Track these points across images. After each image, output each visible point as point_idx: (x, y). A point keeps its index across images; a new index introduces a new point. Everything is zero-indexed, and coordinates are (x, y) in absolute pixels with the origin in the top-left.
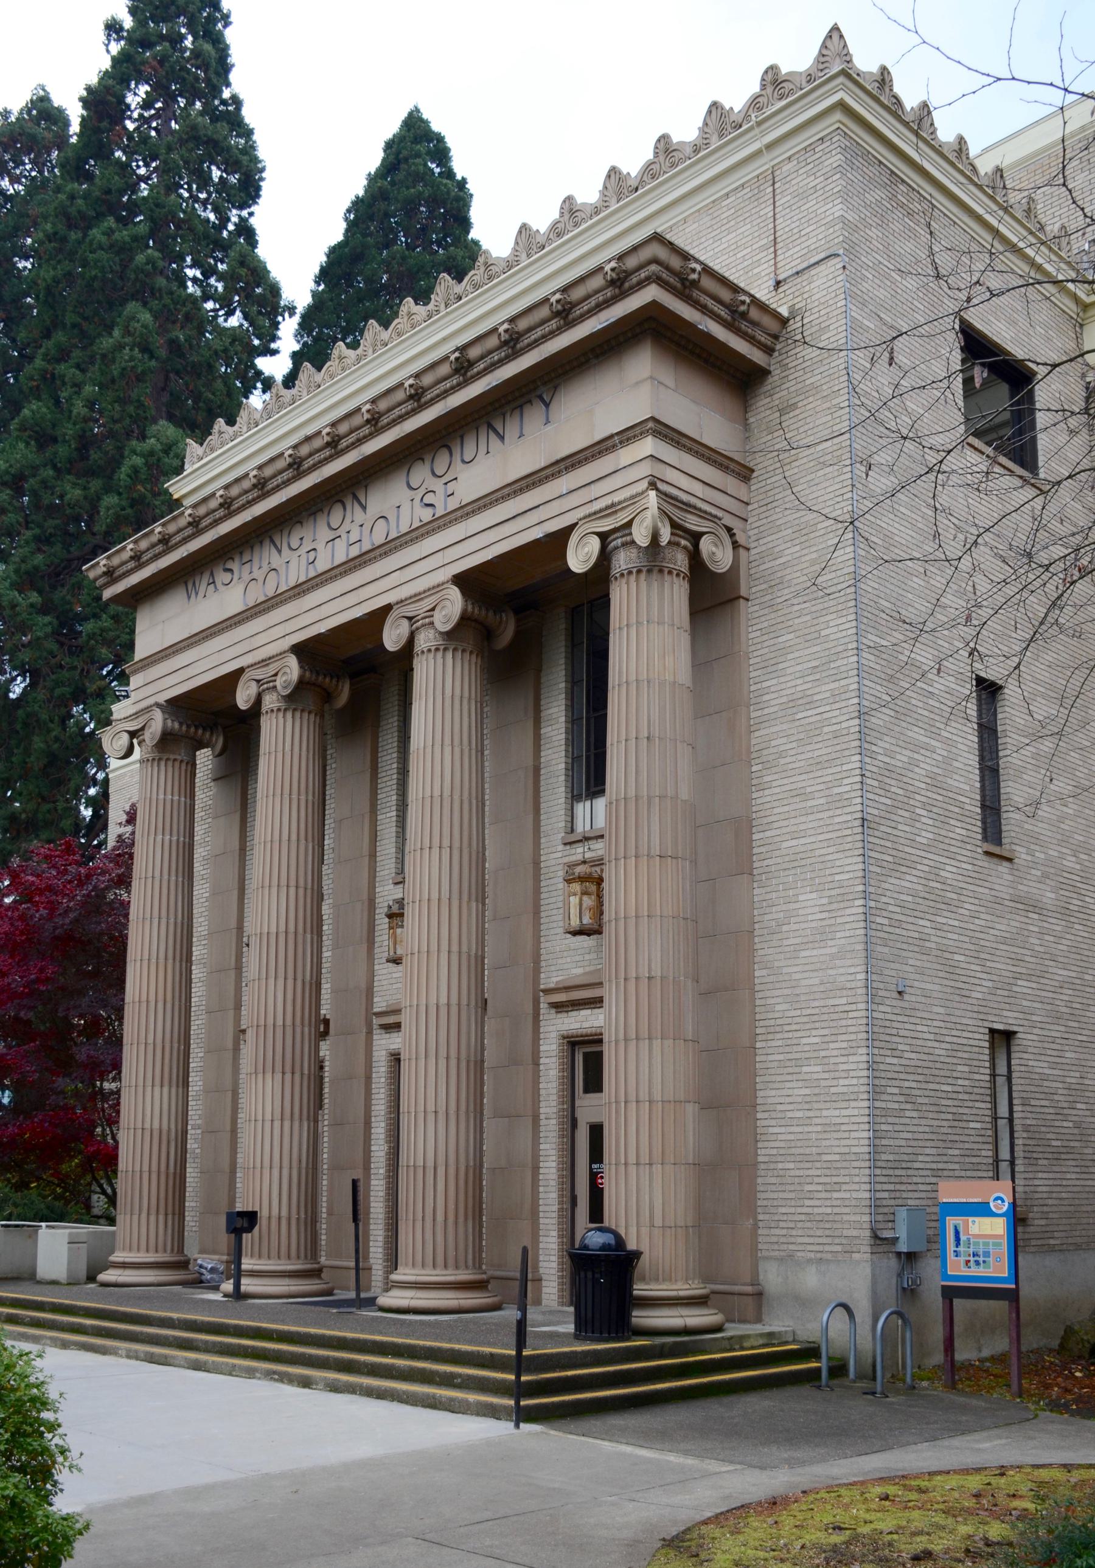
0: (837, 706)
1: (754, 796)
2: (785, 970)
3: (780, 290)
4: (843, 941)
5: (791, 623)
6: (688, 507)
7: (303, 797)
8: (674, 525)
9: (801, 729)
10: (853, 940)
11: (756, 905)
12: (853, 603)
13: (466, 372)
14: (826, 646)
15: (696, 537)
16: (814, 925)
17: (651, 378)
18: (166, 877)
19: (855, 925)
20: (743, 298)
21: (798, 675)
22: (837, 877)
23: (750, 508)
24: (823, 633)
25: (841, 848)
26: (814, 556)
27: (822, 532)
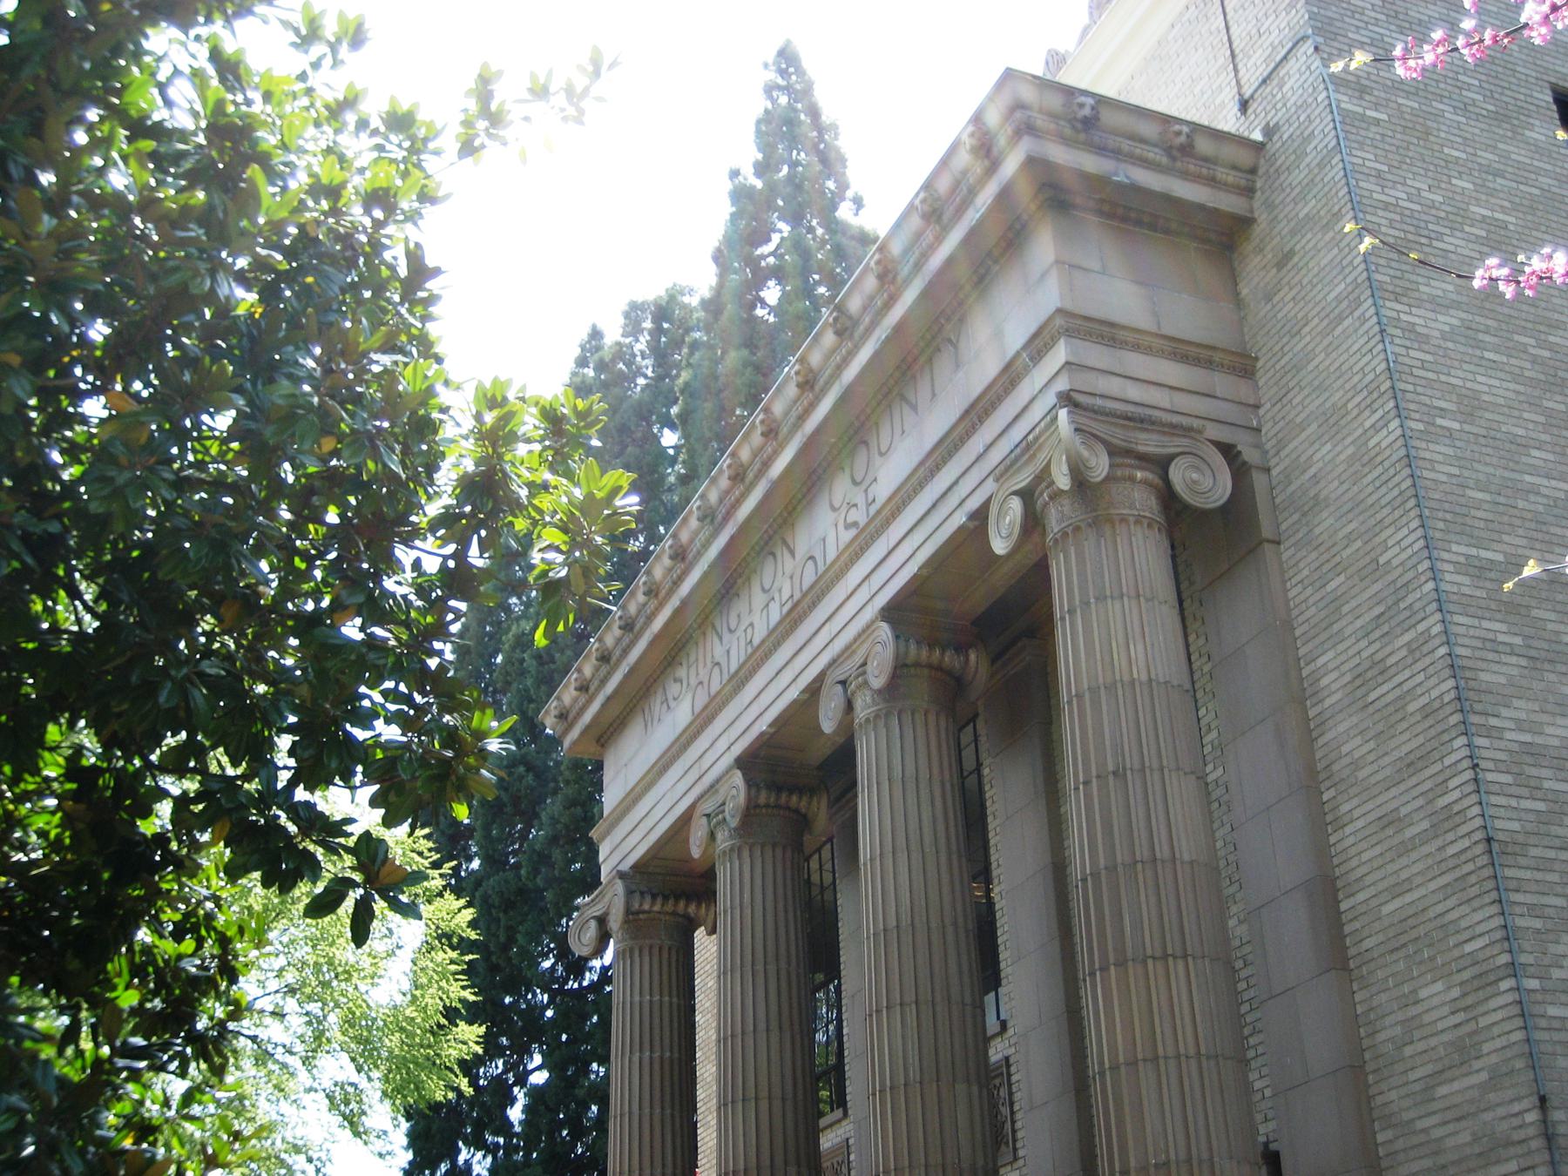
0: (1420, 666)
1: (1332, 840)
2: (1420, 1125)
3: (1250, 111)
4: (1494, 1059)
5: (1338, 559)
6: (1141, 422)
7: (772, 968)
8: (1113, 451)
9: (1377, 717)
10: (1509, 1053)
11: (1361, 1020)
12: (1412, 502)
13: (851, 335)
14: (1390, 578)
15: (1162, 464)
16: (1445, 1037)
17: (1057, 262)
18: (647, 1111)
19: (1507, 1026)
20: (1177, 127)
21: (1360, 634)
22: (1468, 948)
23: (1261, 412)
24: (1382, 560)
25: (1464, 896)
26: (1350, 450)
27: (1355, 412)
